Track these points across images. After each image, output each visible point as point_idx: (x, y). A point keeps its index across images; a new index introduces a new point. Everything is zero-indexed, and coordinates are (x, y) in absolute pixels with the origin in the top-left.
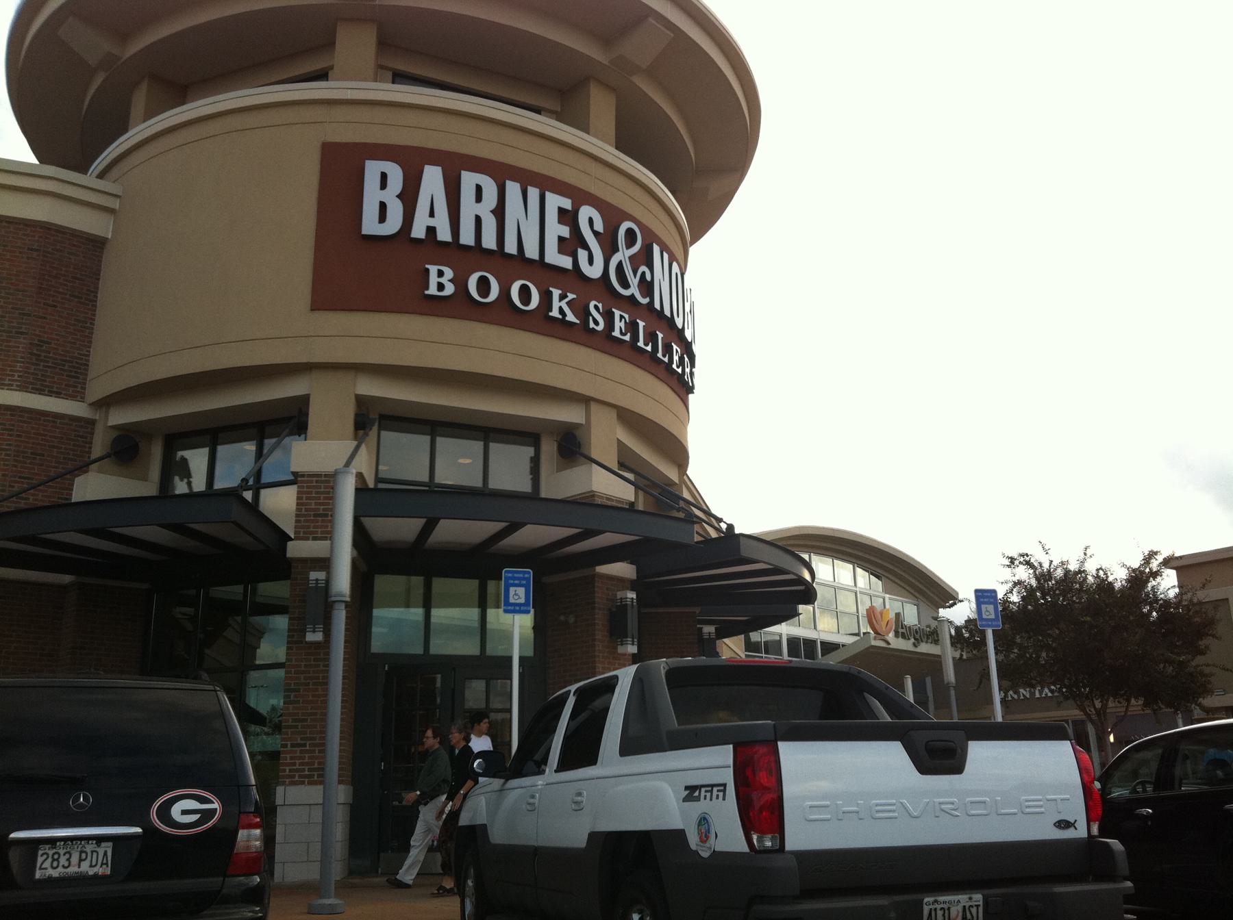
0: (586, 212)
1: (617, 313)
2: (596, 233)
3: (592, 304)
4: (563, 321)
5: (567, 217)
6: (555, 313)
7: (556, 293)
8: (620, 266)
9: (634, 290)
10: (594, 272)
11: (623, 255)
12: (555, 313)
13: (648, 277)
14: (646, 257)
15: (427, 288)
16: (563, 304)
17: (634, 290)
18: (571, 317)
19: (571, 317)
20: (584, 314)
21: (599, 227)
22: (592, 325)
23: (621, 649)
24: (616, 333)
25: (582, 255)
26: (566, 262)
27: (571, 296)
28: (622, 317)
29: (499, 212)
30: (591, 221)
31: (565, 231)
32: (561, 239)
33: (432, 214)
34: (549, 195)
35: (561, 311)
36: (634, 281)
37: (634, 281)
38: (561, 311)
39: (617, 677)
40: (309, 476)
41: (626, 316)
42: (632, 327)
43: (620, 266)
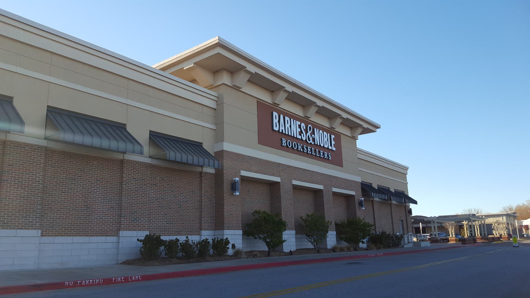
0: (303, 124)
10: (304, 139)
11: (309, 134)
14: (313, 133)
17: (311, 141)
20: (303, 149)
26: (299, 137)
29: (290, 126)
31: (299, 130)
36: (311, 139)
37: (311, 139)
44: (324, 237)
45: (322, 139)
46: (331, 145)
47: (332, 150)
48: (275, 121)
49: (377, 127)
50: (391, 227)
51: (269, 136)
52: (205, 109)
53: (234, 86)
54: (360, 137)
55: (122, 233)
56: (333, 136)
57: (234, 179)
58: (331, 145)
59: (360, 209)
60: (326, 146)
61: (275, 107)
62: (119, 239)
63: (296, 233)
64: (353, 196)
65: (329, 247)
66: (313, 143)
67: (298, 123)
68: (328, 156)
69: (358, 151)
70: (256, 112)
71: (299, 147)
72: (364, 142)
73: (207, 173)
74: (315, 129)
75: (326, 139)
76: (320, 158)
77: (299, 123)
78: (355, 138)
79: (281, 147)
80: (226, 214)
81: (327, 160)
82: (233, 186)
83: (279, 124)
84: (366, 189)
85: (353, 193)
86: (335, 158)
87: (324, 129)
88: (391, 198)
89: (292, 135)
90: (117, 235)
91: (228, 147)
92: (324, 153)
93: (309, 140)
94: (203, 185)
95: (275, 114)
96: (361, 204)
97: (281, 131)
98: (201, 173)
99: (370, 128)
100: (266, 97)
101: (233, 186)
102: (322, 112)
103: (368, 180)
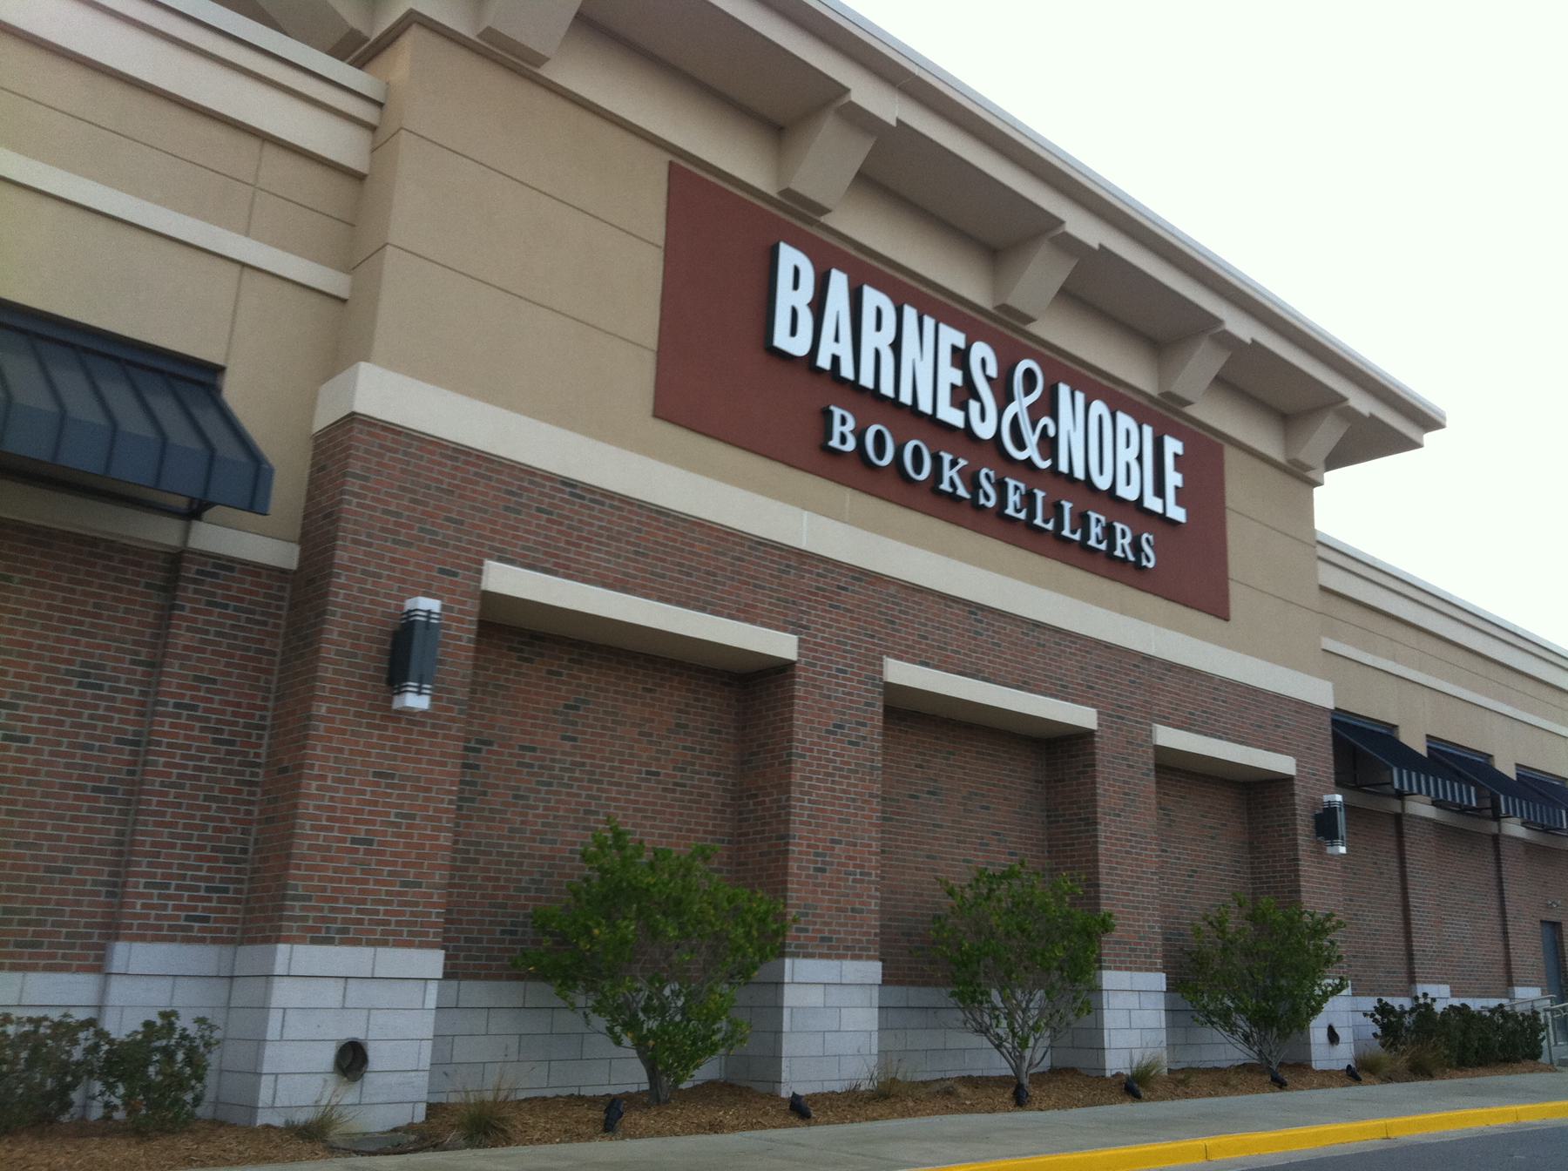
0: (980, 350)
1: (1011, 483)
2: (989, 379)
3: (984, 471)
4: (953, 497)
5: (960, 358)
6: (945, 486)
7: (947, 458)
8: (1015, 422)
9: (1032, 452)
10: (985, 431)
11: (1020, 405)
12: (945, 486)
13: (1051, 432)
14: (1049, 405)
15: (830, 438)
16: (954, 473)
17: (1032, 452)
18: (962, 492)
19: (962, 492)
20: (974, 486)
21: (992, 371)
22: (982, 501)
23: (1330, 850)
24: (1010, 511)
25: (974, 406)
26: (955, 417)
27: (962, 463)
28: (1017, 488)
29: (896, 346)
30: (983, 362)
31: (957, 377)
32: (953, 387)
33: (837, 339)
34: (942, 327)
35: (952, 484)
36: (1032, 439)
37: (1032, 439)
38: (952, 484)
39: (479, 36)
40: (640, 507)
41: (1022, 486)
42: (1029, 500)
43: (1015, 422)
44: (1090, 1003)
45: (1106, 447)
46: (1160, 491)
47: (1162, 518)
48: (791, 298)
49: (1428, 421)
50: (1500, 957)
51: (725, 376)
52: (280, 168)
53: (489, 33)
54: (1330, 477)
55: (125, 954)
56: (1173, 446)
57: (409, 604)
58: (1160, 491)
59: (1320, 852)
60: (1128, 492)
61: (795, 217)
62: (103, 991)
63: (888, 980)
64: (1283, 781)
65: (1117, 1062)
66: (1045, 464)
67: (952, 337)
68: (1136, 546)
69: (1322, 552)
70: (658, 233)
71: (948, 473)
72: (1355, 507)
73: (226, 565)
74: (1064, 390)
75: (1127, 455)
76: (1081, 555)
77: (959, 339)
78: (1303, 478)
79: (826, 461)
80: (308, 835)
81: (1128, 571)
82: (402, 652)
83: (807, 313)
84: (1361, 748)
85: (1283, 764)
86: (1185, 563)
87: (1119, 398)
88: (1495, 807)
89: (906, 398)
90: (99, 966)
91: (382, 392)
92: (1109, 531)
93: (1021, 446)
94: (182, 637)
95: (789, 257)
96: (1325, 825)
97: (824, 362)
98: (176, 559)
99: (1383, 423)
100: (737, 158)
101: (402, 652)
102: (1100, 289)
103: (1375, 705)
